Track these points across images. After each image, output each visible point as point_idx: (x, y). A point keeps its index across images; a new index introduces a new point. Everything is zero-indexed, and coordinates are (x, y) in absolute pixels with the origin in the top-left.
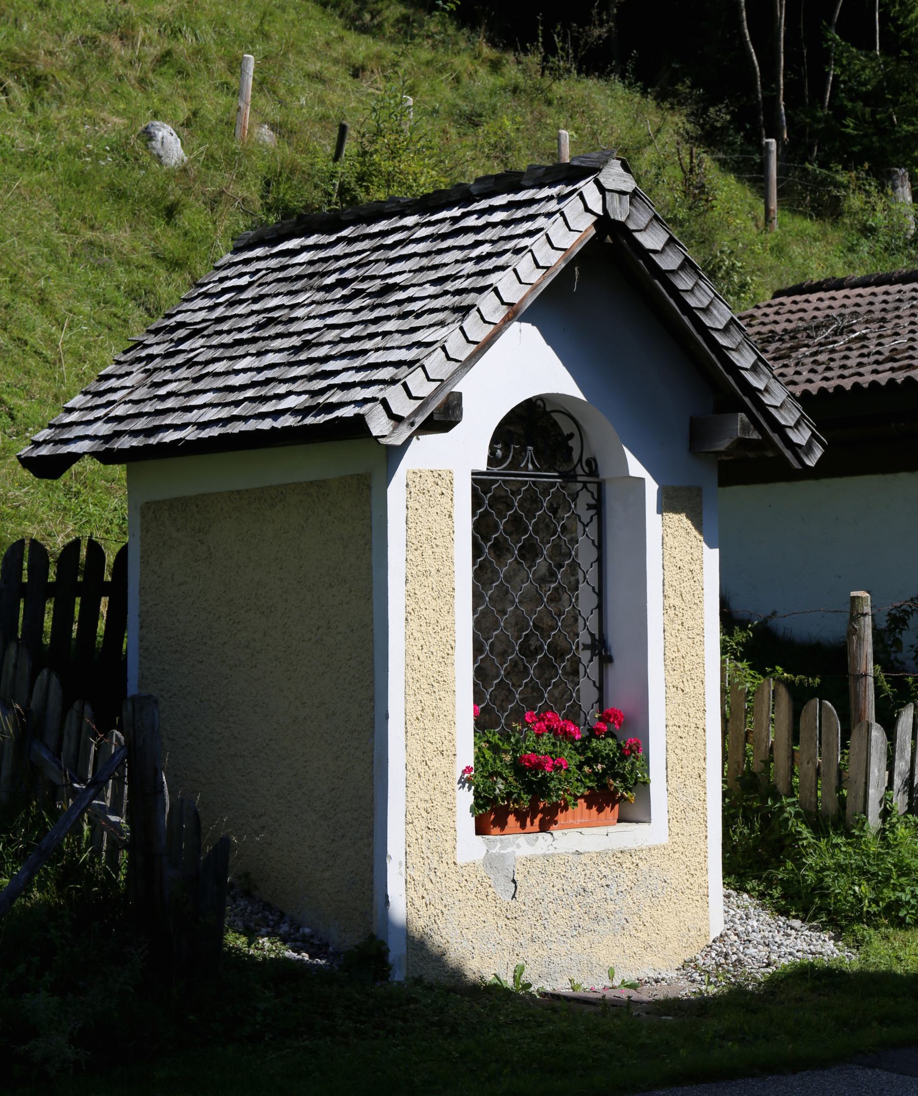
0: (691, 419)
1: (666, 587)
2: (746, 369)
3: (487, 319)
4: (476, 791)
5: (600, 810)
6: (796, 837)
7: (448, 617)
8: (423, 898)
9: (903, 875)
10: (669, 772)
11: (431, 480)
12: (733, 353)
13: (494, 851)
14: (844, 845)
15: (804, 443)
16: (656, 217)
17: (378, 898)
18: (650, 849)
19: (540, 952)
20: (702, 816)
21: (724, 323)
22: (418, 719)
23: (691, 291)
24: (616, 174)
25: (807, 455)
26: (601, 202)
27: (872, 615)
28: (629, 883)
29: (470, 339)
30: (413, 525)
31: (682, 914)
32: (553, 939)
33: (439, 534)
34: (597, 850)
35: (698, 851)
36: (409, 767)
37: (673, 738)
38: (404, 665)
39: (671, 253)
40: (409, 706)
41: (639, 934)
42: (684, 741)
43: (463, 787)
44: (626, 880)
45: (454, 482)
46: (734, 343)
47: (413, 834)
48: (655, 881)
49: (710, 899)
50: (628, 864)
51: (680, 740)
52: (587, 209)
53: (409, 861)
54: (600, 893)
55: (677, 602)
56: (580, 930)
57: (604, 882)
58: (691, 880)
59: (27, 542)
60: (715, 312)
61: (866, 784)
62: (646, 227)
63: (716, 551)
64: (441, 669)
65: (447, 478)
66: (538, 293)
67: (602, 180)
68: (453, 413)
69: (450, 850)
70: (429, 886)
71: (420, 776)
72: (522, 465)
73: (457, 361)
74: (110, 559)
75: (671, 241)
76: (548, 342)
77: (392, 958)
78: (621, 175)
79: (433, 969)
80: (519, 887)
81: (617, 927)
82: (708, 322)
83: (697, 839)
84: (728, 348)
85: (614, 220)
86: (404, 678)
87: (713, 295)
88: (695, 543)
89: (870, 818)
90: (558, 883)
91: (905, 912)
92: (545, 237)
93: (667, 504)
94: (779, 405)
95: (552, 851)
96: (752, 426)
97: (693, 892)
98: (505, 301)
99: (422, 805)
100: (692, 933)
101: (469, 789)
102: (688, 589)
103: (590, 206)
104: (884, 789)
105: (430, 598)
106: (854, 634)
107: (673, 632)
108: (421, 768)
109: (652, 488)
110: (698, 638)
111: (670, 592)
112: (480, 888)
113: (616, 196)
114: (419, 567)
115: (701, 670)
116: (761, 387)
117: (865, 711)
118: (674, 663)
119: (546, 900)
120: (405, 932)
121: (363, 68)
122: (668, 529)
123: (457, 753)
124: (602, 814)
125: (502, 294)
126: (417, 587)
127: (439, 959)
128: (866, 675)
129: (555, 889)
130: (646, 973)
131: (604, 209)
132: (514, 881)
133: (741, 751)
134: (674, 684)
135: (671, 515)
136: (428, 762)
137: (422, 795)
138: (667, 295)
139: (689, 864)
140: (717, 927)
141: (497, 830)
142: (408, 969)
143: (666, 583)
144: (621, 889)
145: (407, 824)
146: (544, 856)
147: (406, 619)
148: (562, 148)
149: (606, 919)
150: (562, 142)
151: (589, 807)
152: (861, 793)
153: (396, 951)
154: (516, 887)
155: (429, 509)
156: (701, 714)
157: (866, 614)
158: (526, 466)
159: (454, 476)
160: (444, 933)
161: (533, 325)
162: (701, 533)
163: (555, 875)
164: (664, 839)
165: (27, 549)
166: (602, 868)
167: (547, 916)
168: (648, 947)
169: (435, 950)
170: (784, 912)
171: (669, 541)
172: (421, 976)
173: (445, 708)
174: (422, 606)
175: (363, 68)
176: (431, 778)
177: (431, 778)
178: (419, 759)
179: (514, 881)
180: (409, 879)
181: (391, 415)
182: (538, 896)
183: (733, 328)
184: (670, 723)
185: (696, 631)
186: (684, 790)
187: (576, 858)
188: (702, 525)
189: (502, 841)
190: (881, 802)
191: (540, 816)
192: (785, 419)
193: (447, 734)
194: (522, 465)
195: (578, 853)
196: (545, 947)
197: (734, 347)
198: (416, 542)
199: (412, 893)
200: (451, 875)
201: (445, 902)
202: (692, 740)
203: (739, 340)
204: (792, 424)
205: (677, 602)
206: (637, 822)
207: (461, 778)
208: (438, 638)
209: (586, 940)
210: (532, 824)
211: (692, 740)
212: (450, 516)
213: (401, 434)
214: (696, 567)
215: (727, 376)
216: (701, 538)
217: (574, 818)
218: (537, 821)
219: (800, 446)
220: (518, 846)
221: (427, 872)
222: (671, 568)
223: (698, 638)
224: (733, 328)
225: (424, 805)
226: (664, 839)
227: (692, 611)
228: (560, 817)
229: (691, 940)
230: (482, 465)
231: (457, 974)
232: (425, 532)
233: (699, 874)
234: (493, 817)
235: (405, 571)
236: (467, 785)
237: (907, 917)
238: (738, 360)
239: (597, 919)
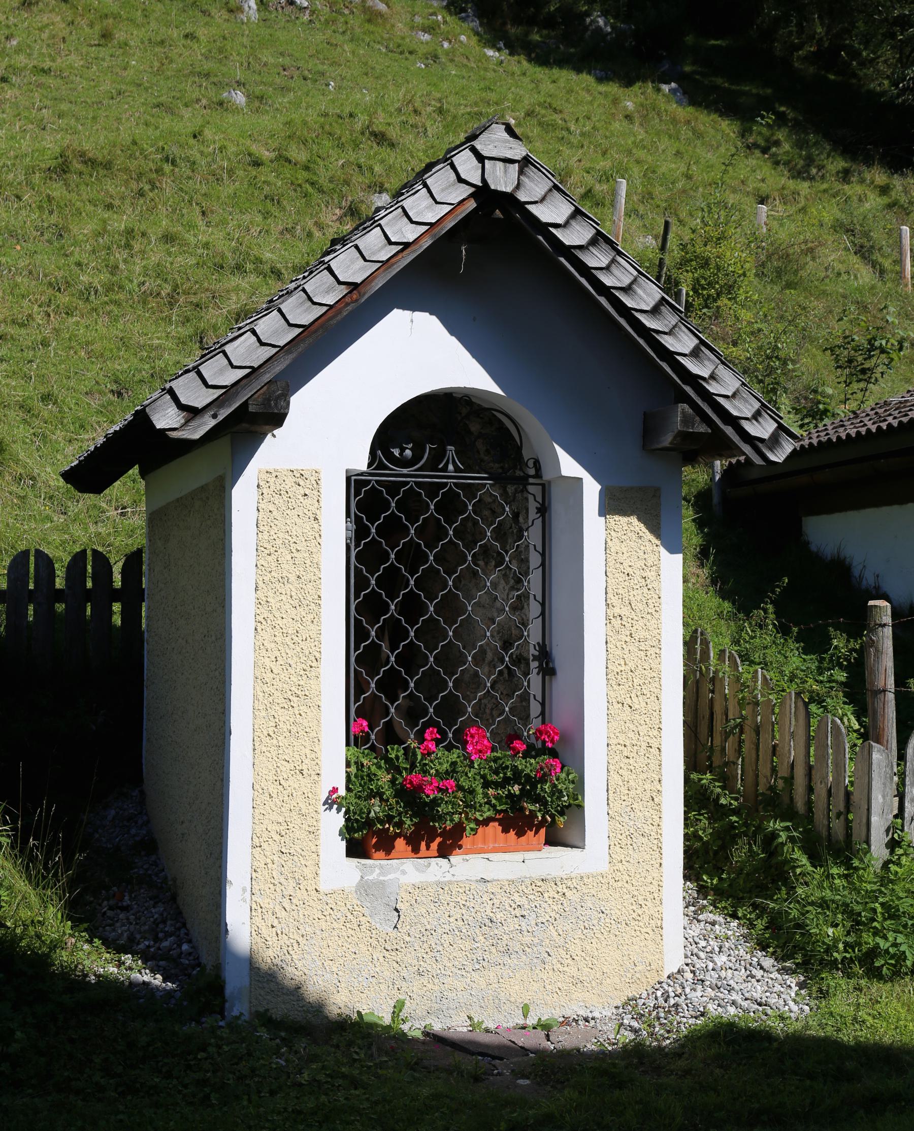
0: (645, 414)
1: (610, 595)
2: (684, 355)
3: (315, 300)
4: (346, 813)
5: (520, 834)
6: (791, 864)
7: (312, 627)
8: (273, 927)
9: (891, 917)
10: (611, 795)
11: (290, 481)
12: (666, 337)
13: (371, 878)
14: (839, 878)
15: (766, 436)
16: (555, 187)
17: (223, 924)
18: (582, 877)
19: (430, 986)
20: (656, 842)
22: (269, 735)
23: (607, 268)
24: (499, 140)
25: (771, 449)
26: (480, 171)
27: (893, 626)
28: (553, 914)
29: (291, 322)
30: (267, 528)
31: (626, 947)
32: (448, 973)
33: (301, 538)
34: (510, 878)
35: (649, 879)
36: (257, 787)
37: (617, 758)
38: (252, 678)
39: (578, 227)
40: (258, 721)
41: (566, 969)
42: (631, 761)
43: (330, 808)
44: (549, 910)
45: (322, 483)
46: (666, 326)
47: (263, 860)
48: (589, 912)
49: (664, 932)
50: (552, 893)
51: (627, 761)
52: (460, 180)
53: (255, 886)
54: (513, 924)
55: (625, 611)
56: (485, 964)
57: (518, 912)
58: (640, 912)
60: (639, 291)
61: (869, 810)
62: (543, 200)
63: (679, 557)
64: (301, 683)
65: (313, 479)
66: (394, 273)
67: (478, 147)
68: (276, 404)
69: (310, 876)
70: (282, 914)
71: (271, 797)
72: (440, 466)
73: (274, 346)
74: (117, 570)
75: (577, 213)
76: (452, 332)
77: (229, 989)
78: (506, 141)
79: (284, 1003)
80: (401, 919)
81: (535, 960)
82: (629, 302)
83: (649, 868)
84: (658, 332)
85: (496, 191)
86: (252, 691)
87: (635, 273)
88: (649, 548)
89: (873, 847)
90: (457, 913)
91: (883, 962)
92: (400, 210)
94: (730, 394)
95: (448, 877)
96: (698, 418)
97: (641, 924)
98: (341, 279)
99: (274, 828)
100: (640, 968)
101: (339, 810)
103: (463, 176)
104: (891, 817)
105: (288, 606)
106: (871, 647)
107: (618, 644)
108: (273, 789)
109: (592, 490)
110: (652, 651)
111: (614, 600)
112: (350, 916)
113: (500, 165)
114: (273, 574)
115: (657, 685)
116: (705, 373)
117: (884, 729)
118: (619, 677)
119: (440, 931)
120: (251, 964)
121: (767, 197)
122: (613, 533)
123: (322, 772)
124: (523, 839)
125: (336, 273)
126: (270, 594)
127: (296, 992)
128: (884, 691)
129: (452, 920)
130: (575, 1009)
131: (483, 180)
132: (396, 910)
133: (769, 766)
134: (619, 699)
135: (617, 518)
136: (282, 782)
137: (275, 817)
138: (576, 274)
139: (636, 893)
140: (673, 960)
141: (381, 854)
142: (251, 1002)
143: (610, 590)
144: (540, 920)
145: (254, 847)
146: (438, 883)
147: (256, 629)
148: (903, 240)
149: (521, 952)
150: (903, 236)
151: (505, 830)
152: (864, 820)
153: (235, 981)
154: (399, 916)
155: (288, 512)
156: (656, 733)
157: (884, 625)
158: (445, 469)
159: (322, 476)
160: (299, 965)
161: (431, 314)
162: (658, 536)
163: (452, 904)
164: (603, 866)
165: (32, 559)
166: (516, 897)
167: (440, 948)
168: (577, 982)
170: (763, 947)
171: (614, 546)
172: (267, 1010)
173: (307, 725)
174: (277, 614)
175: (767, 197)
176: (286, 798)
177: (286, 798)
178: (271, 777)
179: (396, 910)
180: (254, 906)
181: (181, 407)
182: (428, 927)
183: (665, 309)
184: (613, 741)
185: (649, 643)
186: (632, 814)
187: (481, 886)
188: (659, 528)
189: (381, 867)
190: (887, 831)
191: (439, 840)
192: (739, 410)
193: (308, 752)
194: (440, 466)
195: (484, 881)
196: (436, 981)
197: (667, 330)
198: (269, 547)
199: (258, 920)
200: (311, 903)
201: (302, 931)
202: (642, 761)
203: (674, 323)
204: (749, 415)
205: (625, 611)
206: (572, 847)
207: (328, 798)
208: (299, 649)
209: (492, 974)
210: (428, 848)
211: (642, 761)
212: (316, 519)
213: (199, 426)
214: (651, 574)
215: (661, 363)
216: (658, 542)
217: (484, 841)
218: (434, 846)
219: (762, 440)
220: (404, 872)
221: (279, 899)
222: (617, 575)
223: (652, 651)
224: (665, 309)
225: (278, 828)
226: (603, 866)
227: (645, 621)
229: (638, 975)
230: (361, 463)
231: (318, 1008)
232: (281, 535)
233: (649, 904)
234: (374, 840)
235: (255, 577)
236: (335, 806)
237: (885, 968)
238: (672, 345)
239: (507, 952)
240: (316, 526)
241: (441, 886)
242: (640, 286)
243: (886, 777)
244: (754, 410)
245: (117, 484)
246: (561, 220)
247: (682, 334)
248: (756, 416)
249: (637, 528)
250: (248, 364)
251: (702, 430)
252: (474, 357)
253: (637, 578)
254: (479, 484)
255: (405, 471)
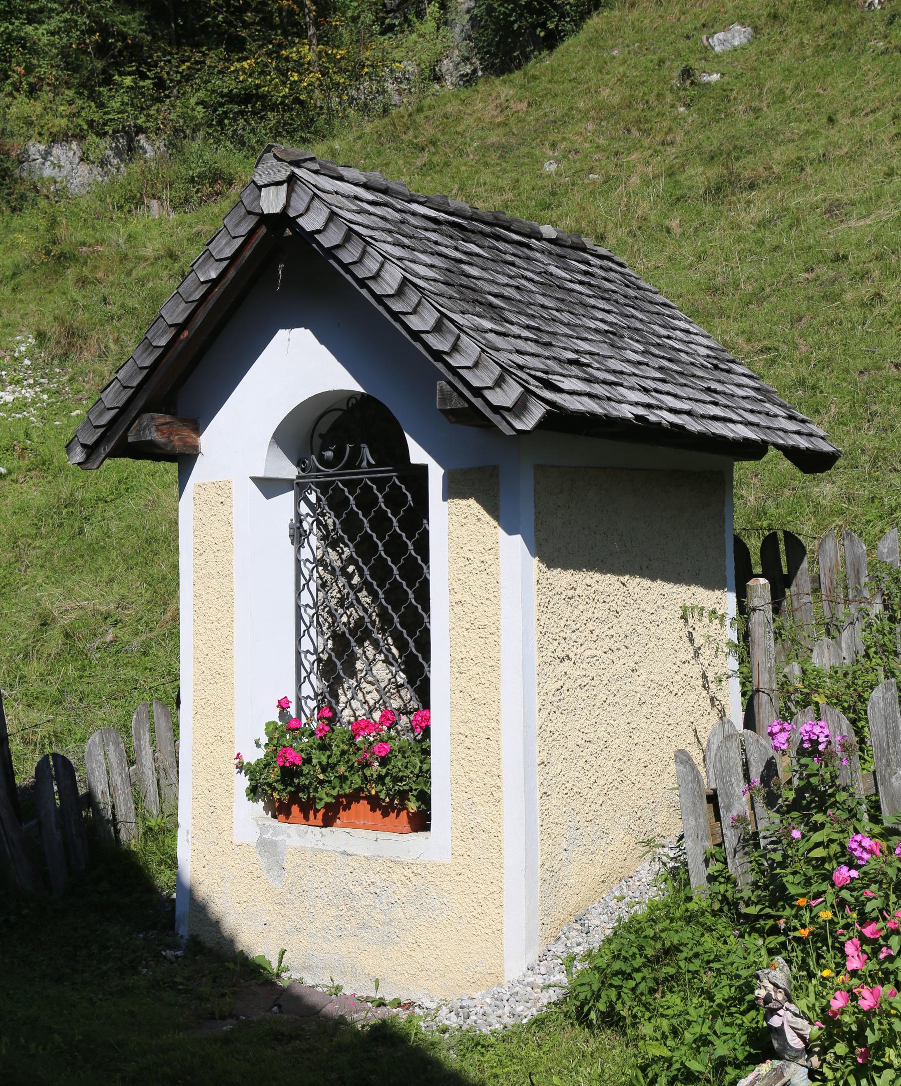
21: (395, 286)
25: (518, 417)
42: (472, 752)
43: (241, 772)
46: (410, 305)
51: (467, 751)
59: (781, 535)
62: (307, 209)
63: (518, 538)
73: (132, 388)
81: (386, 939)
82: (378, 291)
93: (451, 491)
94: (470, 365)
102: (478, 583)
109: (436, 475)
127: (216, 925)
135: (456, 501)
158: (359, 467)
162: (496, 517)
169: (214, 917)
172: (198, 935)
197: (410, 310)
204: (490, 384)
216: (496, 524)
219: (507, 409)
220: (289, 836)
223: (491, 639)
228: (342, 814)
231: (231, 942)
240: (229, 528)
241: (316, 852)
242: (387, 272)
243: (694, 795)
244: (494, 378)
245: (752, 462)
246: (318, 226)
247: (426, 311)
248: (499, 382)
249: (476, 511)
250: (116, 405)
251: (459, 406)
252: (339, 361)
253: (476, 564)
254: (328, 482)
255: (331, 471)
